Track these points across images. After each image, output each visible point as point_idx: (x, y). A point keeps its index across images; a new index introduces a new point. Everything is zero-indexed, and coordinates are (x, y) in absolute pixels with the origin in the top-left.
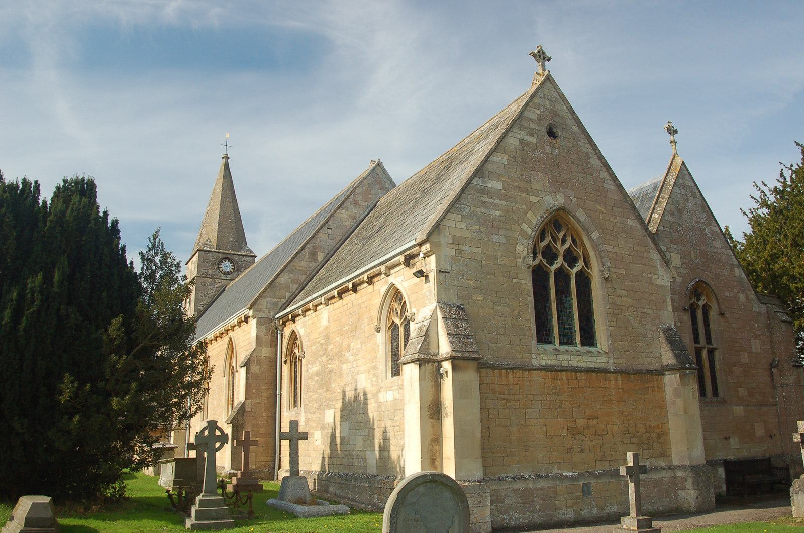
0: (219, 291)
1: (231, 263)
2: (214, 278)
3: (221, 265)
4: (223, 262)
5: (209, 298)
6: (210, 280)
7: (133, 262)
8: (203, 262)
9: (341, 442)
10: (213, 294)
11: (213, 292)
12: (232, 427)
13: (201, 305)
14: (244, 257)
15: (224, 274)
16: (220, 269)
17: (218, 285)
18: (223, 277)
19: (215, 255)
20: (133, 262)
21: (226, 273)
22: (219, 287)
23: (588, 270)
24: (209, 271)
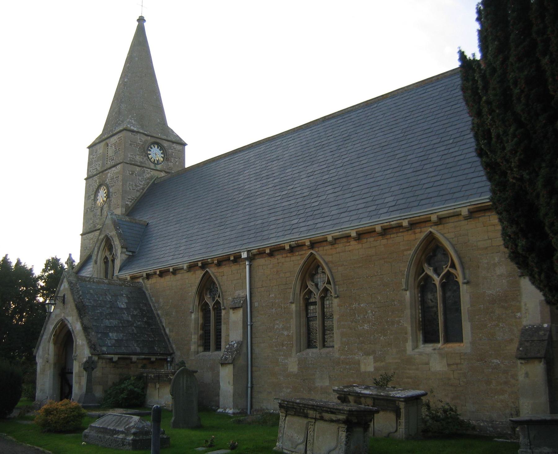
0: (148, 183)
1: (160, 150)
2: (143, 167)
3: (150, 151)
4: (152, 148)
5: (137, 191)
6: (138, 169)
7: (463, 52)
8: (131, 144)
9: (413, 389)
10: (142, 186)
11: (142, 183)
12: (35, 396)
13: (129, 199)
14: (174, 145)
15: (154, 162)
16: (150, 156)
17: (148, 176)
18: (152, 166)
19: (144, 138)
20: (463, 52)
21: (156, 162)
22: (148, 178)
23: (76, 327)
24: (138, 157)
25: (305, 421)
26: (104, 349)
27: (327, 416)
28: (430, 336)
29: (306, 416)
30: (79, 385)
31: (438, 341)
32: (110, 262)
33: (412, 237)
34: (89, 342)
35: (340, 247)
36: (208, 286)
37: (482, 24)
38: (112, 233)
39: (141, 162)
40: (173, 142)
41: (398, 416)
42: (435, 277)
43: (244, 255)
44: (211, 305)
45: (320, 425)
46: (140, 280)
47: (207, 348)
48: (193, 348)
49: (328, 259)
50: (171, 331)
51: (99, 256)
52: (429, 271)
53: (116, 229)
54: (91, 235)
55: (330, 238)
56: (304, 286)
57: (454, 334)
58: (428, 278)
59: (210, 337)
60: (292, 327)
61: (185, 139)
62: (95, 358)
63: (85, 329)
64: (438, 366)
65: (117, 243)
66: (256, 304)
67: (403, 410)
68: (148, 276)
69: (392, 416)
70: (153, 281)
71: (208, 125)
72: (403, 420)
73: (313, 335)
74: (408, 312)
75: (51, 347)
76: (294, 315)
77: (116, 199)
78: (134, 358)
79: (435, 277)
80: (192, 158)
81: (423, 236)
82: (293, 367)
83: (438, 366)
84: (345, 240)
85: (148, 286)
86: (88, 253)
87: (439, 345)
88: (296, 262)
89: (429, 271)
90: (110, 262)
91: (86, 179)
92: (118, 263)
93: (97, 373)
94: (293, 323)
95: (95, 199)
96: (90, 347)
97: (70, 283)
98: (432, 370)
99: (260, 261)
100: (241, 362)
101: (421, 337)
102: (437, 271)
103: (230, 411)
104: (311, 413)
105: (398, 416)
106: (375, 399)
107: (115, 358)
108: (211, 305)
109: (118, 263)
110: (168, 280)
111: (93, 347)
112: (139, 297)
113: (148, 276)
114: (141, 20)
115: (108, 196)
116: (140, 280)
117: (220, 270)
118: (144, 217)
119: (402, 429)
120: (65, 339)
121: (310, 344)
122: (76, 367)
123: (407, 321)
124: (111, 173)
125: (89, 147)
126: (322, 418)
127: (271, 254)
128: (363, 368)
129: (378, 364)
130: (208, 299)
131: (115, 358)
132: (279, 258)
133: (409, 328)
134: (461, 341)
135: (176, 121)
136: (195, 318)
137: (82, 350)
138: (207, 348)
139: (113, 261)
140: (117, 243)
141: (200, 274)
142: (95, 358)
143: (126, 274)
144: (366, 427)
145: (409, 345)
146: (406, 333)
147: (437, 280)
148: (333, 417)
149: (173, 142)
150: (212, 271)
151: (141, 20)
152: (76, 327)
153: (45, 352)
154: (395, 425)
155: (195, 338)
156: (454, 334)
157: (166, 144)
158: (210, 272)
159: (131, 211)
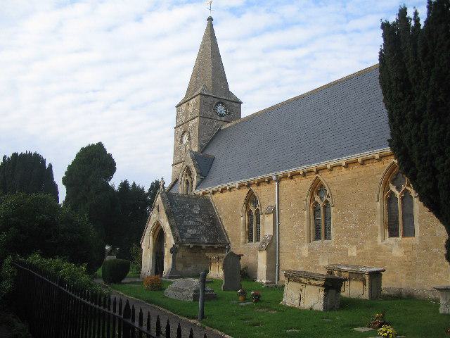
6: (209, 120)
23: (166, 225)
25: (299, 285)
26: (184, 240)
27: (313, 282)
28: (393, 232)
29: (300, 282)
30: (168, 264)
31: (397, 236)
32: (190, 184)
33: (382, 166)
34: (174, 235)
35: (336, 171)
36: (251, 199)
37: (385, 40)
38: (191, 164)
39: (211, 116)
40: (233, 102)
41: (365, 284)
42: (397, 192)
43: (274, 178)
44: (321, 204)
45: (309, 287)
46: (209, 195)
47: (250, 239)
48: (242, 240)
49: (327, 180)
50: (228, 229)
51: (182, 179)
52: (317, 198)
53: (194, 162)
54: (179, 165)
55: (328, 167)
56: (312, 198)
57: (409, 232)
58: (392, 193)
59: (252, 233)
60: (304, 225)
61: (241, 99)
62: (177, 246)
63: (172, 227)
64: (398, 252)
65: (194, 171)
66: (282, 211)
67: (367, 281)
68: (214, 193)
69: (361, 284)
70: (217, 195)
71: (257, 86)
72: (367, 287)
73: (320, 231)
74: (379, 216)
75: (151, 238)
76: (379, 212)
77: (195, 139)
78: (204, 246)
79: (397, 192)
80: (246, 112)
81: (389, 164)
82: (305, 253)
83: (398, 252)
84: (338, 168)
85: (214, 199)
86: (175, 178)
87: (400, 238)
88: (307, 183)
89: (393, 188)
90: (190, 184)
91: (175, 128)
92: (195, 184)
93: (179, 255)
94: (305, 224)
95: (181, 141)
96: (175, 239)
97: (162, 197)
98: (232, 250)
99: (284, 182)
100: (272, 249)
101: (387, 233)
102: (398, 188)
103: (264, 281)
104: (303, 280)
105: (365, 284)
106: (351, 273)
107: (191, 246)
108: (321, 204)
109: (195, 184)
110: (226, 194)
111: (176, 238)
112: (206, 204)
113: (214, 193)
114: (210, 19)
115: (189, 139)
116: (209, 195)
117: (259, 188)
118: (208, 152)
119: (367, 293)
120: (160, 236)
121: (317, 237)
122: (167, 251)
123: (378, 222)
124: (191, 123)
125: (177, 107)
126: (310, 284)
127: (291, 178)
128: (350, 254)
129: (359, 251)
130: (252, 207)
131: (191, 246)
132: (297, 179)
133: (379, 228)
134: (414, 236)
135: (235, 88)
136: (242, 219)
137: (170, 241)
138: (250, 239)
139: (192, 182)
140: (194, 171)
141: (245, 191)
142: (177, 246)
143: (199, 192)
144: (338, 290)
145: (379, 239)
146: (377, 230)
147: (398, 194)
148: (316, 282)
149: (233, 102)
150: (254, 188)
151: (210, 19)
152: (166, 225)
153: (147, 243)
154: (362, 290)
155: (242, 234)
156: (409, 232)
157: (227, 103)
158: (321, 178)
159: (203, 148)
